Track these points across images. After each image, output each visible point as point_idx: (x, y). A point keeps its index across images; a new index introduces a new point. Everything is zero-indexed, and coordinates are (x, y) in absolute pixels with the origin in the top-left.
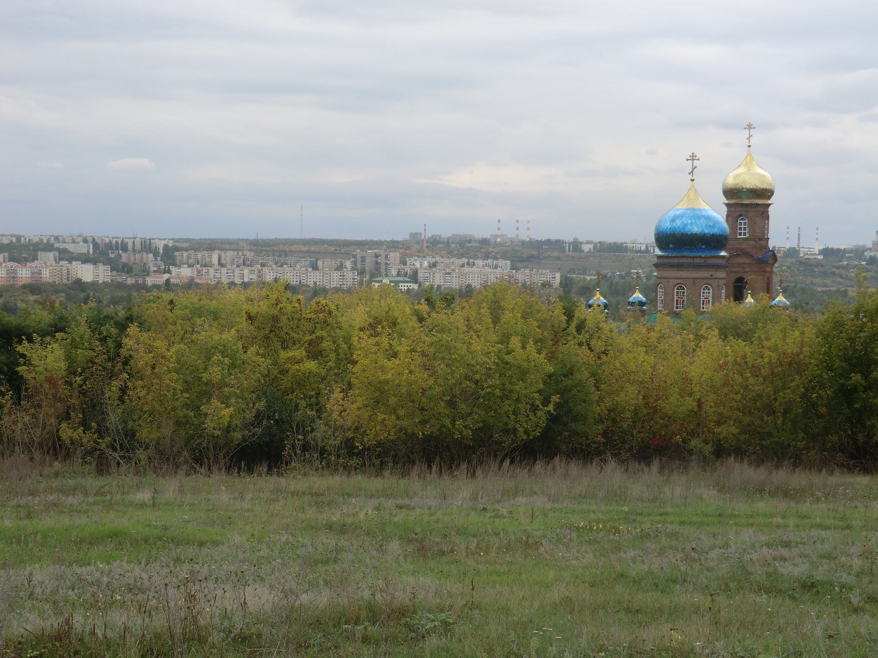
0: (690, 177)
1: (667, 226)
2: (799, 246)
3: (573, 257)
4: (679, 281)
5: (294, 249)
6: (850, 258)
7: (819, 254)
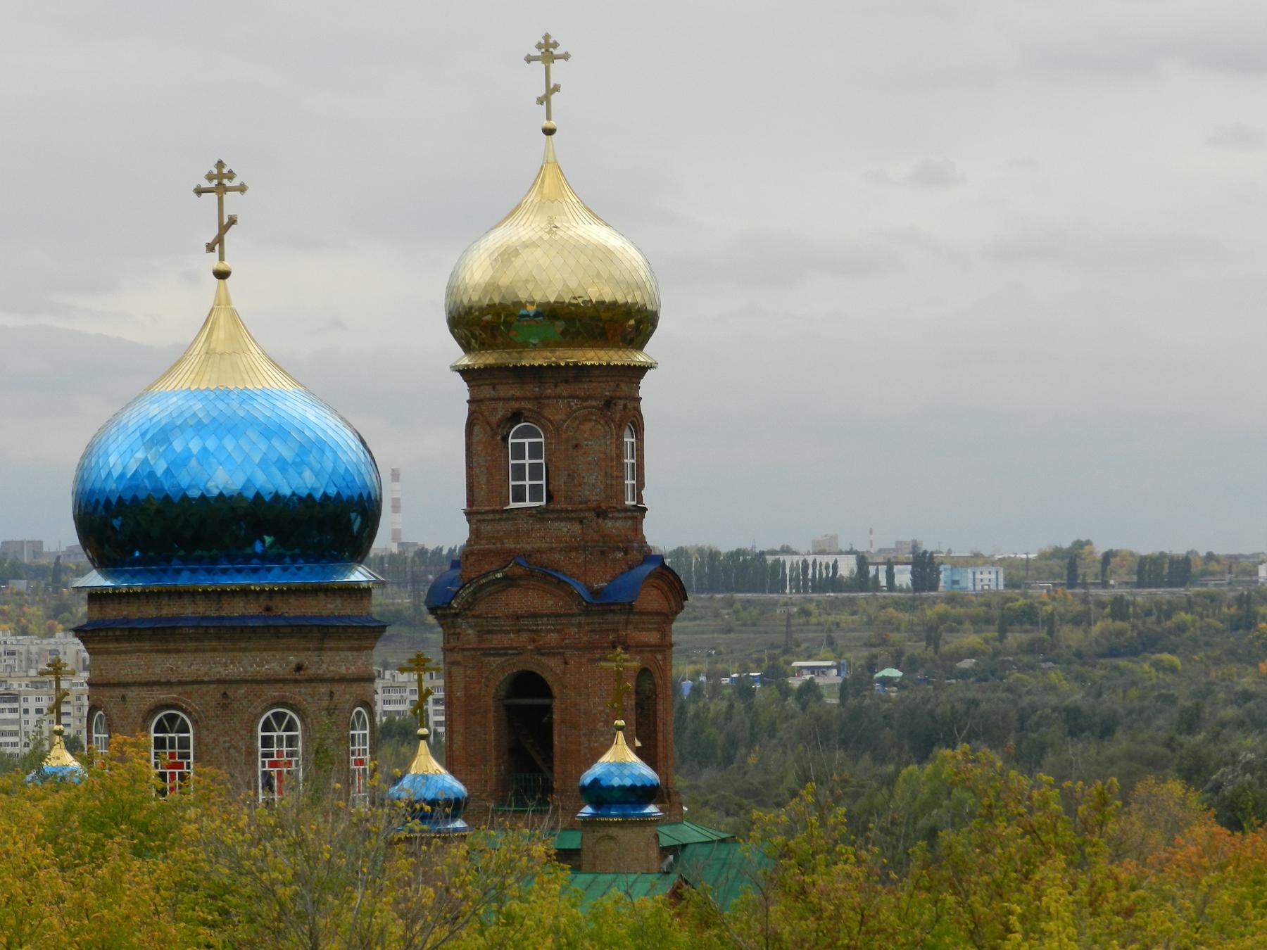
1: (122, 461)
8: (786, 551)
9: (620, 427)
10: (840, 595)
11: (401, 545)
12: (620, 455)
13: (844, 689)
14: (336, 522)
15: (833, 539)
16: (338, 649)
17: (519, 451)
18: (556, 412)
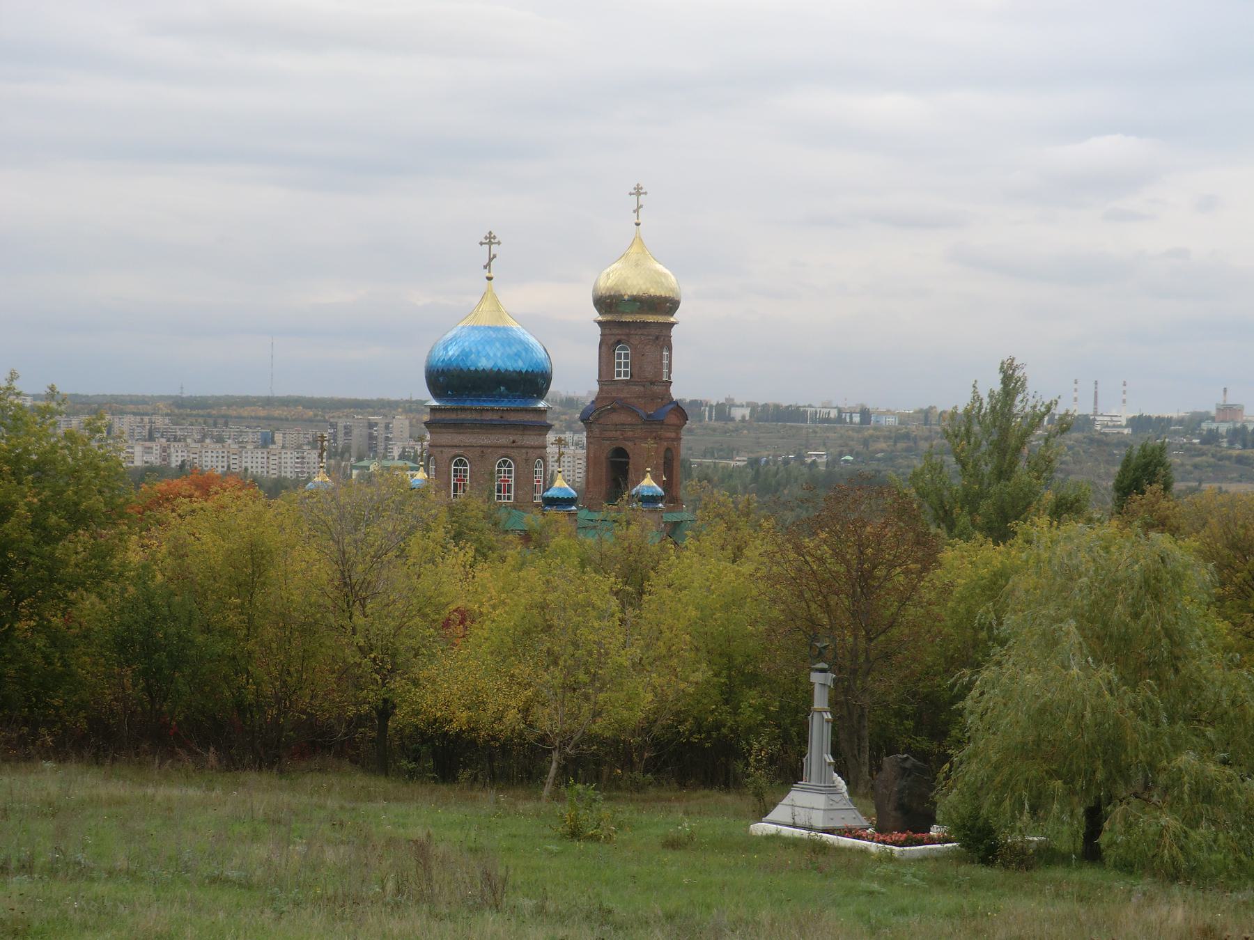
2: (1095, 414)
3: (714, 430)
4: (458, 451)
5: (245, 414)
6: (1176, 432)
7: (1126, 427)
8: (810, 406)
9: (662, 348)
12: (661, 360)
13: (827, 464)
14: (533, 382)
17: (619, 356)
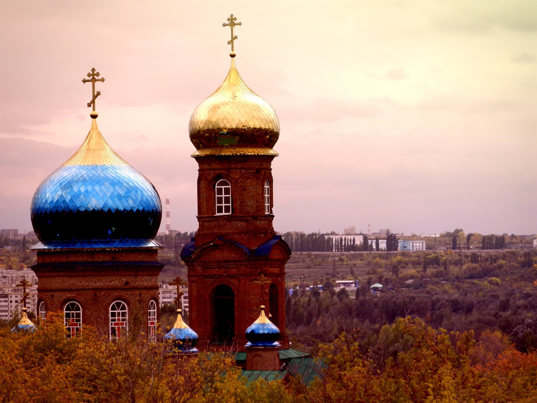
0: (90, 111)
1: (52, 195)
4: (69, 295)
8: (333, 234)
10: (356, 253)
11: (170, 231)
12: (263, 193)
13: (358, 292)
14: (146, 219)
15: (353, 229)
16: (143, 275)
17: (220, 191)
18: (236, 175)
